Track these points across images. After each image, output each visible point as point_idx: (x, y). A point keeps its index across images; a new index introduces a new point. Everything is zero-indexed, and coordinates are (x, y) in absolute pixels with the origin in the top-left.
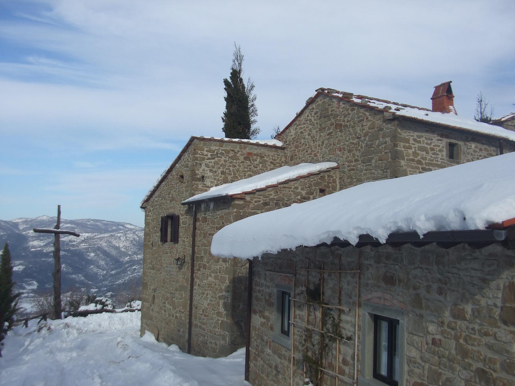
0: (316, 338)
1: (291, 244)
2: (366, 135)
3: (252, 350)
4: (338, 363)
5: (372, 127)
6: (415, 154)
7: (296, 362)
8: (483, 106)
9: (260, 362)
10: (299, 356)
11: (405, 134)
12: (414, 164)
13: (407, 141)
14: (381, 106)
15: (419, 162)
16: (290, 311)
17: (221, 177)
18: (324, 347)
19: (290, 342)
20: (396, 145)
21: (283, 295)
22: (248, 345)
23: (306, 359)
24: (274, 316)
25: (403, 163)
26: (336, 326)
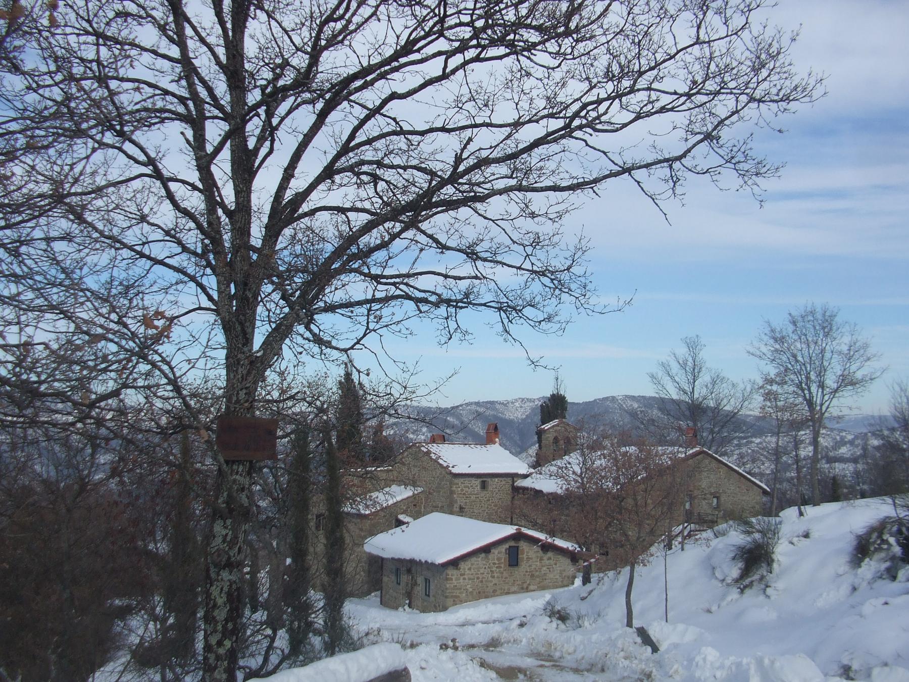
0: (410, 585)
1: (402, 557)
2: (438, 477)
3: (383, 594)
4: (416, 593)
5: (441, 474)
6: (462, 490)
7: (403, 594)
8: (559, 384)
9: (388, 596)
10: (404, 592)
11: (456, 481)
12: (461, 496)
13: (458, 484)
14: (445, 464)
15: (464, 494)
16: (628, 613)
17: (227, 326)
18: (412, 588)
19: (401, 587)
20: (451, 487)
21: (397, 570)
22: (381, 589)
23: (406, 592)
24: (393, 578)
25: (455, 496)
26: (416, 581)
